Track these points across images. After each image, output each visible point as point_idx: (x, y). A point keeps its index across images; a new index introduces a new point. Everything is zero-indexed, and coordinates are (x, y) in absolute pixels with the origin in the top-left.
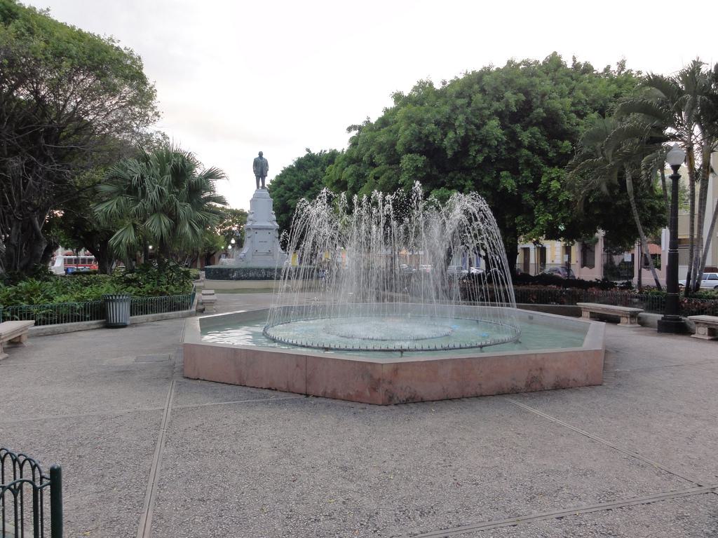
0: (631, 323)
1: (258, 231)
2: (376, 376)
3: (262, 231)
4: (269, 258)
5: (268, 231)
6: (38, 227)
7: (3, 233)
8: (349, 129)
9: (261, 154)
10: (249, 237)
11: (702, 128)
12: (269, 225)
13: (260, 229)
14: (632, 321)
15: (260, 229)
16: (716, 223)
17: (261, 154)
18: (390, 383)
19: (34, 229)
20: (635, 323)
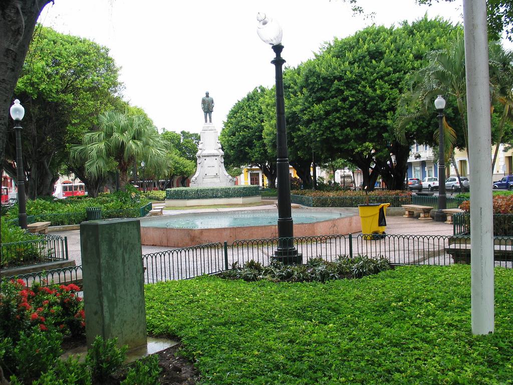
0: (425, 217)
1: (207, 158)
2: (193, 235)
3: (210, 158)
4: (220, 174)
5: (215, 158)
6: (46, 165)
7: (195, 384)
8: (326, 43)
9: (207, 95)
10: (200, 164)
11: (242, 165)
12: (216, 152)
13: (208, 156)
14: (426, 216)
15: (208, 156)
16: (493, 158)
17: (207, 95)
18: (199, 238)
19: (44, 167)
20: (428, 217)
